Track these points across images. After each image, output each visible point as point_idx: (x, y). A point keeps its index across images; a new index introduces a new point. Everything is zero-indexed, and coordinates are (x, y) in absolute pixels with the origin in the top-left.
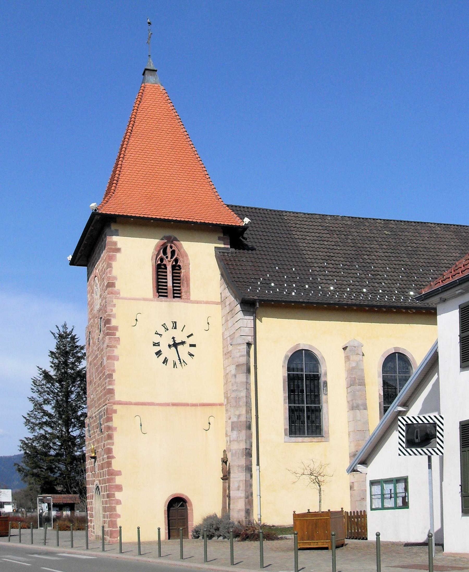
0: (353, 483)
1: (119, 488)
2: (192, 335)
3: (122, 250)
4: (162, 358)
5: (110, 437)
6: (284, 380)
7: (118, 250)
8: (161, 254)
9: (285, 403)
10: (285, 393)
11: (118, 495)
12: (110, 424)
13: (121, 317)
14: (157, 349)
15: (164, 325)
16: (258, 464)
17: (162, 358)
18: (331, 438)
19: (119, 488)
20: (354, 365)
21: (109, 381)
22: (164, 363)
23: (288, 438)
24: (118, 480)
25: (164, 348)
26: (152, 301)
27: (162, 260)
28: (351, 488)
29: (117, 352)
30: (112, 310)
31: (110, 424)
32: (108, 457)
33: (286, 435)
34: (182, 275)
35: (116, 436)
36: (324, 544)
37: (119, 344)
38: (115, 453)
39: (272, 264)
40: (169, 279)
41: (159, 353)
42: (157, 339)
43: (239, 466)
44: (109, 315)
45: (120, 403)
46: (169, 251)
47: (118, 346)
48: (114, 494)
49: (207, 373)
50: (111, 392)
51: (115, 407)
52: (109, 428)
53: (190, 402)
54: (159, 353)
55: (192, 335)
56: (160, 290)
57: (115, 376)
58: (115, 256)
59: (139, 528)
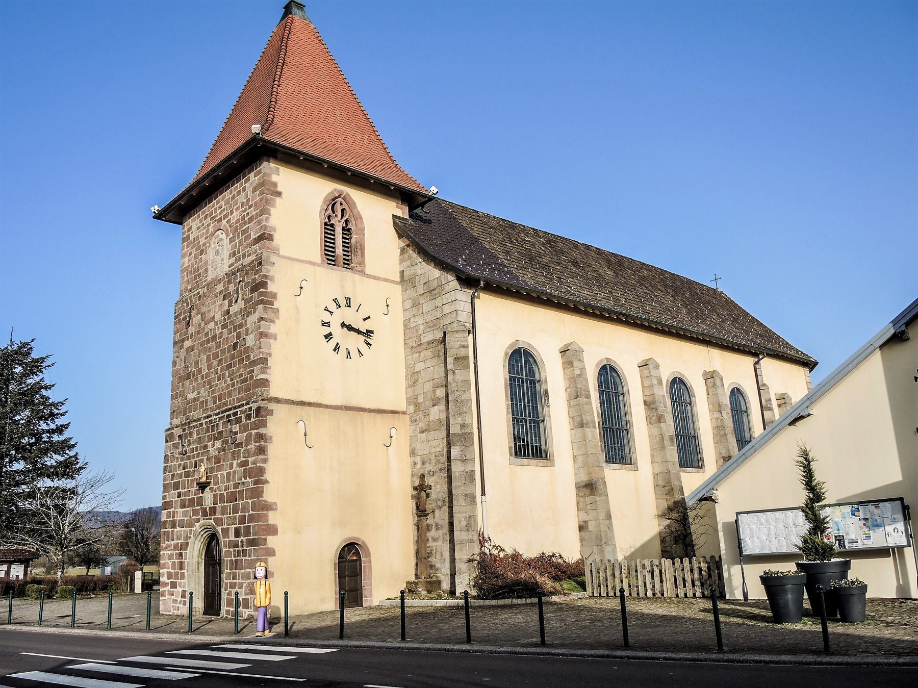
0: (586, 522)
1: (273, 530)
2: (369, 317)
3: (283, 194)
4: (332, 344)
5: (262, 450)
6: (506, 383)
7: (279, 194)
8: (330, 211)
9: (508, 413)
10: (507, 400)
11: (272, 541)
12: (262, 431)
13: (281, 281)
14: (326, 330)
15: (335, 300)
16: (483, 494)
17: (332, 344)
18: (557, 462)
19: (273, 530)
20: (577, 372)
21: (263, 368)
22: (335, 350)
23: (513, 458)
24: (273, 518)
25: (336, 329)
26: (319, 265)
27: (329, 217)
28: (581, 528)
29: (273, 329)
30: (269, 271)
31: (262, 431)
32: (256, 483)
33: (511, 455)
34: (353, 240)
35: (272, 449)
36: (229, 604)
37: (278, 318)
38: (267, 476)
39: (459, 247)
40: (340, 245)
41: (328, 336)
42: (327, 317)
43: (466, 496)
44: (266, 276)
45: (277, 400)
46: (338, 208)
47: (277, 321)
48: (265, 540)
49: (385, 373)
50: (265, 383)
51: (272, 406)
52: (261, 437)
53: (367, 407)
54: (328, 336)
55: (369, 317)
56: (330, 257)
57: (270, 362)
58: (274, 201)
59: (286, 594)
